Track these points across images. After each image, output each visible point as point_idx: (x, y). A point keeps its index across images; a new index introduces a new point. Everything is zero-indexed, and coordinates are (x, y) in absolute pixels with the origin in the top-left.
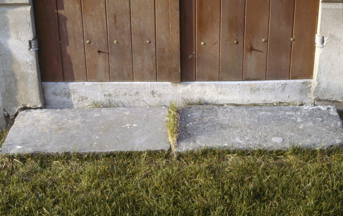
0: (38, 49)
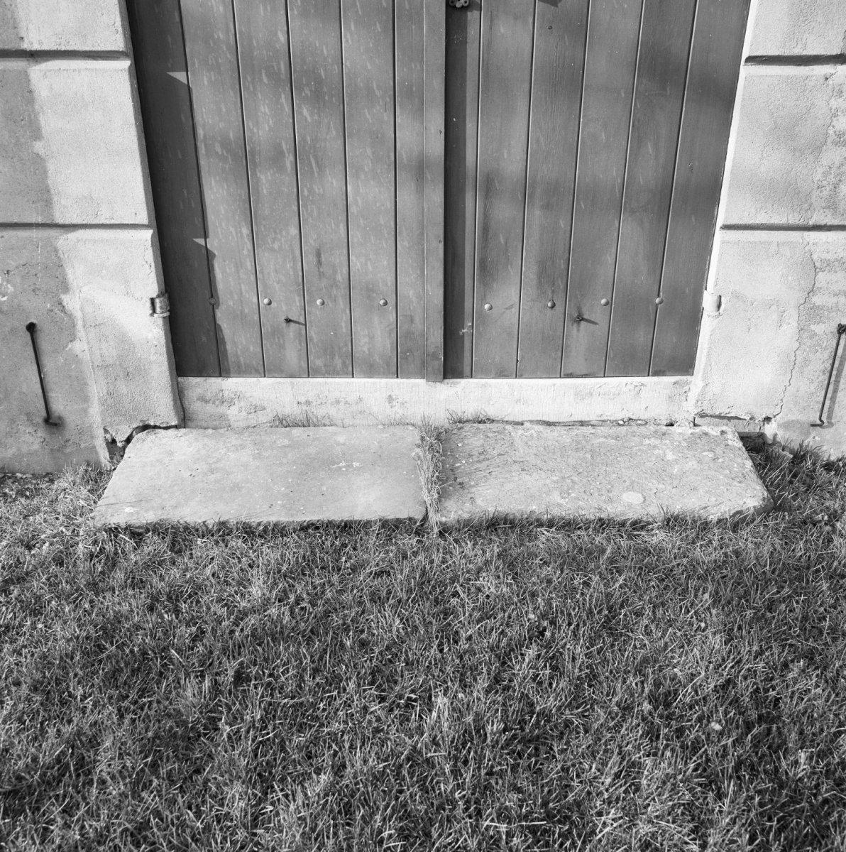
0: (168, 314)
